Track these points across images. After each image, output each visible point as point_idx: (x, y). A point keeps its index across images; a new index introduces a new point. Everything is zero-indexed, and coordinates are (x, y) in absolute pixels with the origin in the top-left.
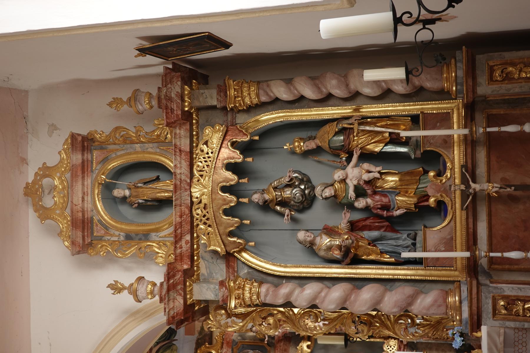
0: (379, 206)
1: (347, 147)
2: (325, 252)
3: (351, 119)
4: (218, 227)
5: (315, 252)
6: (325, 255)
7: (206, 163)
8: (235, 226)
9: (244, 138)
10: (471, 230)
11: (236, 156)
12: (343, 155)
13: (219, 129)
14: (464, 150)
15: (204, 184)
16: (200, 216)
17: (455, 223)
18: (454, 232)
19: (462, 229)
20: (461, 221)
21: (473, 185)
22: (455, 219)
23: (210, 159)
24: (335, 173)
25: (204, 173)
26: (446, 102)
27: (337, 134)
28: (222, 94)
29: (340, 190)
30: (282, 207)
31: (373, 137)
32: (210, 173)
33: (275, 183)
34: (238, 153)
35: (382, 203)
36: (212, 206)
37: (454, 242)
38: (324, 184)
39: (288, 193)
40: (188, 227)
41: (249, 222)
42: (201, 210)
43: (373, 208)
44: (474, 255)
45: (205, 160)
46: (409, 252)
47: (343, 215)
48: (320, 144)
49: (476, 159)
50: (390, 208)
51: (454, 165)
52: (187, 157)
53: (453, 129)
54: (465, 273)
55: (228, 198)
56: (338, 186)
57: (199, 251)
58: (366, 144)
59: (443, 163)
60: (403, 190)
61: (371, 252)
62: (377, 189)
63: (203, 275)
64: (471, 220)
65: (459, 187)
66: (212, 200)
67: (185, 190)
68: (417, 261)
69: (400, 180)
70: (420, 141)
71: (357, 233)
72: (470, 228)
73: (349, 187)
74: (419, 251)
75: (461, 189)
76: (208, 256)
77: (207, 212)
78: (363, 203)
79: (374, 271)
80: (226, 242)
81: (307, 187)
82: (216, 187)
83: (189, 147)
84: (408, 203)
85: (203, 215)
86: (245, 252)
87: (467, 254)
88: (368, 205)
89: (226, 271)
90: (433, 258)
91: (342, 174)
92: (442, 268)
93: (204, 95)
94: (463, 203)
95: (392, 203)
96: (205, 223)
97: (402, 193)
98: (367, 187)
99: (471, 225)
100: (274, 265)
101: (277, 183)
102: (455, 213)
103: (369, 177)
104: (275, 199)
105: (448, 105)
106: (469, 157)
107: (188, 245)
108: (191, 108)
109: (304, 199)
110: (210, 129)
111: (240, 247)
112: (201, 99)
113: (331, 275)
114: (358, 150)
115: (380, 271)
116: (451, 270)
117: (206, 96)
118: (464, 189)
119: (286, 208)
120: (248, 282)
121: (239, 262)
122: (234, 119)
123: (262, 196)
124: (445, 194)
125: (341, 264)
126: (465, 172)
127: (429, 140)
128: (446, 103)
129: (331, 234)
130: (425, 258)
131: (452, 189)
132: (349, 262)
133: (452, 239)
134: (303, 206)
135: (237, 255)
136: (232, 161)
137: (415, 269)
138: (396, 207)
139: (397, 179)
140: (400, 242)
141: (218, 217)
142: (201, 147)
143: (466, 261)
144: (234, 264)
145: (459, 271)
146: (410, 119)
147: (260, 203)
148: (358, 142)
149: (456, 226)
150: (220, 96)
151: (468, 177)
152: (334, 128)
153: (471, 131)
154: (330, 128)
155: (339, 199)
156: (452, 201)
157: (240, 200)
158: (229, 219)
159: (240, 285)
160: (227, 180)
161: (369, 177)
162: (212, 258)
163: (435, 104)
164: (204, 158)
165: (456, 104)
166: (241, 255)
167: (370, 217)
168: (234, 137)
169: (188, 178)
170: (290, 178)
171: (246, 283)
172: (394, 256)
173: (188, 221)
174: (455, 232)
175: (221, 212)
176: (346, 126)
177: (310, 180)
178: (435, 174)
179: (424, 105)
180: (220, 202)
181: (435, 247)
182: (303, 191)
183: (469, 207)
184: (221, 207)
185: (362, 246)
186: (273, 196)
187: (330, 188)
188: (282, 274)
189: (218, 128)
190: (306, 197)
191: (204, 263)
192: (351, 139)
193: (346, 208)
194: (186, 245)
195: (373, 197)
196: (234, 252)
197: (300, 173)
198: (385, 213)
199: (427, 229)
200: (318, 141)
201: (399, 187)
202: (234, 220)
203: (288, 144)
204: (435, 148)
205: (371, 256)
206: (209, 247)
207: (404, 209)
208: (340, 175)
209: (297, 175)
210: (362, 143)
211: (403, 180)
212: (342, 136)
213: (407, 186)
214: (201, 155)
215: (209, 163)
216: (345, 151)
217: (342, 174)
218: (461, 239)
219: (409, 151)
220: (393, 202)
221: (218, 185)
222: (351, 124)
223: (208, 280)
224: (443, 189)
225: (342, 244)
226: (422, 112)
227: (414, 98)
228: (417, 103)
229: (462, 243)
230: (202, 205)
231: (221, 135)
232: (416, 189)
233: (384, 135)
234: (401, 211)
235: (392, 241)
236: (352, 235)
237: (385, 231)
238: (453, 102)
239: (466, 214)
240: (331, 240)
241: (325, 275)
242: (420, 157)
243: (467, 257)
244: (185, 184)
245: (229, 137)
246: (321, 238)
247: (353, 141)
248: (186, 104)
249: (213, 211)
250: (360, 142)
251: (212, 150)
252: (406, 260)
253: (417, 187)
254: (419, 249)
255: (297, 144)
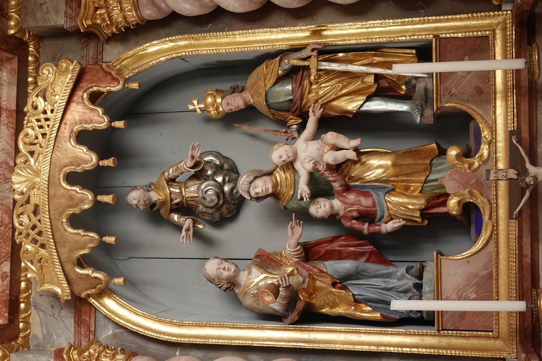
0: (355, 214)
1: (298, 103)
2: (253, 299)
3: (303, 50)
4: (58, 248)
5: (239, 299)
6: (254, 305)
7: (40, 130)
8: (90, 248)
9: (112, 86)
10: (528, 260)
11: (96, 118)
12: (293, 120)
13: (67, 69)
14: (515, 106)
15: (35, 167)
16: (26, 227)
17: (497, 247)
18: (494, 263)
19: (509, 257)
20: (508, 241)
21: (532, 170)
22: (497, 238)
23: (48, 123)
24: (273, 150)
25: (37, 148)
26: (481, 16)
27: (280, 80)
28: (74, 4)
29: (285, 184)
30: (182, 215)
31: (345, 83)
32: (47, 148)
33: (171, 172)
34: (101, 112)
35: (361, 208)
36: (49, 208)
37: (494, 282)
38: (255, 171)
39: (192, 189)
40: (7, 248)
41: (114, 239)
42: (28, 216)
43: (344, 217)
44: (535, 307)
45: (39, 123)
46: (410, 299)
47: (289, 230)
48: (252, 101)
49: (538, 123)
50: (376, 217)
51: (496, 135)
52: (10, 119)
53: (495, 59)
54: (514, 343)
55: (78, 195)
56: (281, 177)
57: (30, 294)
58: (333, 97)
59: (474, 134)
60: (400, 184)
61: (337, 301)
62: (353, 182)
63: (36, 337)
64: (527, 241)
65: (504, 174)
66: (48, 198)
67: (5, 180)
68: (423, 318)
69: (394, 165)
70: (431, 89)
71: (314, 265)
72: (526, 256)
73: (300, 177)
74: (428, 299)
75: (509, 177)
76: (44, 303)
77: (39, 221)
78: (325, 206)
79: (342, 337)
80: (72, 276)
81: (227, 179)
82: (57, 174)
83: (15, 102)
84: (409, 208)
85: (31, 225)
86: (110, 297)
87: (520, 306)
88: (334, 213)
89: (75, 332)
90: (454, 313)
91: (286, 151)
92: (470, 333)
93: (44, 7)
94: (512, 206)
95: (378, 208)
96: (35, 241)
97: (397, 190)
98: (332, 177)
99: (527, 251)
100: (160, 321)
101: (173, 172)
102: (497, 226)
103: (336, 158)
104: (169, 200)
105: (487, 22)
106: (525, 118)
107: (5, 282)
108: (22, 31)
109: (221, 202)
110: (50, 69)
111: (98, 287)
112: (38, 15)
113: (261, 343)
114: (318, 108)
115: (354, 337)
116: (488, 337)
117: (48, 8)
118: (515, 177)
119: (186, 217)
120: (107, 353)
121: (99, 315)
122: (100, 54)
123: (145, 195)
124: (478, 191)
125: (283, 322)
126: (517, 145)
127: (449, 88)
128: (482, 18)
129: (267, 266)
130: (438, 312)
131: (492, 177)
132: (296, 318)
133: (491, 276)
134: (221, 214)
135: (93, 300)
136: (89, 126)
137: (419, 335)
138: (386, 214)
139: (389, 163)
140: (393, 283)
141: (59, 230)
142: (34, 100)
143: (516, 320)
144: (90, 319)
145: (504, 340)
146: (415, 52)
147: (140, 207)
148: (317, 93)
149: (497, 251)
150: (71, 8)
151: (523, 153)
152: (275, 69)
153: (529, 64)
154: (268, 69)
155: (283, 201)
156: (490, 204)
157: (100, 198)
158: (78, 234)
159: (90, 358)
160: (78, 161)
161: (336, 158)
162: (53, 307)
163: (461, 19)
164: (38, 120)
165: (500, 19)
166: (101, 301)
167: (341, 236)
168: (94, 85)
169: (12, 160)
170: (194, 161)
171: (103, 354)
172: (381, 308)
173: (6, 238)
174: (497, 263)
175: (64, 221)
176: (296, 62)
177: (236, 168)
178: (459, 151)
179: (440, 21)
180: (64, 201)
181: (459, 291)
182: (221, 186)
183: (524, 215)
184: (64, 211)
185: (322, 288)
186: (165, 195)
187: (265, 178)
188: (173, 338)
189: (64, 65)
190: (224, 198)
191: (38, 317)
192: (305, 87)
193: (294, 218)
194: (3, 281)
195: (344, 197)
196: (89, 296)
197: (218, 155)
198: (365, 228)
199: (444, 257)
200: (247, 95)
201: (392, 179)
202: (88, 235)
203: (195, 102)
204: (461, 102)
205: (338, 309)
206: (41, 287)
207: (401, 220)
208: (283, 153)
209: (212, 158)
210: (326, 94)
211: (400, 165)
212: (289, 84)
213: (408, 177)
214: (34, 115)
215: (47, 130)
216: (295, 112)
217: (286, 151)
218: (509, 277)
219: (412, 109)
220: (381, 205)
221: (61, 170)
222: (304, 59)
223: (44, 347)
224: (474, 180)
225: (281, 282)
226: (436, 36)
227: (422, 11)
228: (426, 18)
229: (509, 285)
230: (30, 208)
231: (70, 79)
232: (425, 183)
233: (366, 80)
234: (395, 223)
235: (379, 280)
236: (304, 268)
237: (367, 261)
238: (494, 16)
239: (517, 228)
240: (266, 277)
241: (250, 342)
242: (433, 123)
243: (520, 312)
244: (6, 169)
245: (85, 84)
246: (250, 273)
247: (310, 92)
248: (12, 23)
249: (50, 218)
250: (321, 92)
251: (53, 106)
252: (403, 316)
253: (426, 179)
254: (427, 295)
255: (210, 100)
